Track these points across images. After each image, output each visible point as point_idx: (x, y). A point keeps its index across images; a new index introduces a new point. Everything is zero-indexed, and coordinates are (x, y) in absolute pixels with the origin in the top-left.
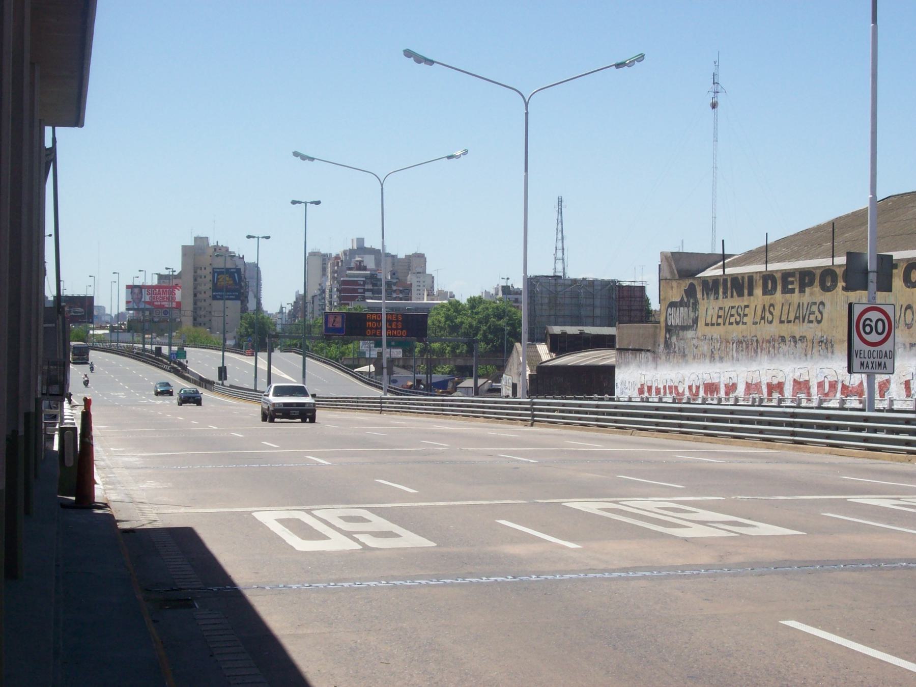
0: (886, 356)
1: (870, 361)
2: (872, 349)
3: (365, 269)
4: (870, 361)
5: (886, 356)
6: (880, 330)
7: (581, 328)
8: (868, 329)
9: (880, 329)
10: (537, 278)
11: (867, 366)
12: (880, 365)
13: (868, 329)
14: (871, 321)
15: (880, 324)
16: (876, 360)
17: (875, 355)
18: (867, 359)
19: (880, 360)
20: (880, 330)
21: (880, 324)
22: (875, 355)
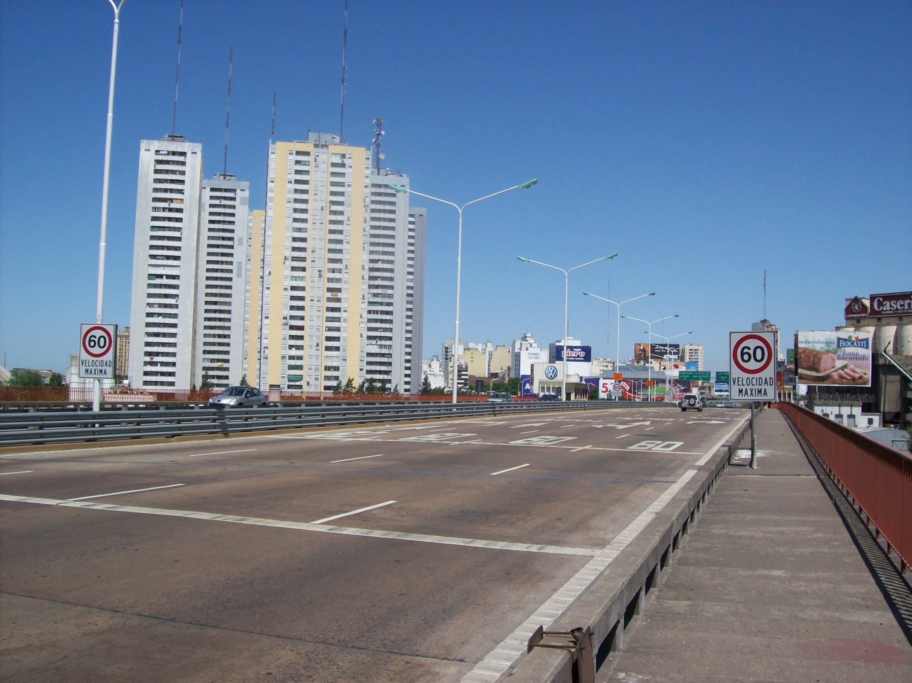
0: (766, 382)
1: (93, 368)
2: (95, 359)
3: (817, 370)
4: (748, 388)
5: (766, 382)
6: (102, 345)
7: (649, 509)
8: (746, 357)
9: (102, 344)
10: (259, 208)
11: (746, 393)
12: (101, 371)
13: (746, 357)
14: (749, 348)
15: (102, 340)
16: (755, 387)
17: (754, 382)
18: (746, 386)
19: (760, 387)
20: (102, 345)
21: (102, 340)
22: (754, 382)
